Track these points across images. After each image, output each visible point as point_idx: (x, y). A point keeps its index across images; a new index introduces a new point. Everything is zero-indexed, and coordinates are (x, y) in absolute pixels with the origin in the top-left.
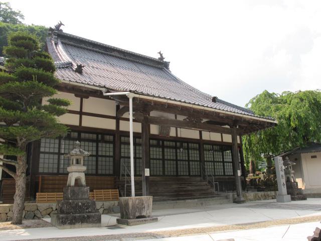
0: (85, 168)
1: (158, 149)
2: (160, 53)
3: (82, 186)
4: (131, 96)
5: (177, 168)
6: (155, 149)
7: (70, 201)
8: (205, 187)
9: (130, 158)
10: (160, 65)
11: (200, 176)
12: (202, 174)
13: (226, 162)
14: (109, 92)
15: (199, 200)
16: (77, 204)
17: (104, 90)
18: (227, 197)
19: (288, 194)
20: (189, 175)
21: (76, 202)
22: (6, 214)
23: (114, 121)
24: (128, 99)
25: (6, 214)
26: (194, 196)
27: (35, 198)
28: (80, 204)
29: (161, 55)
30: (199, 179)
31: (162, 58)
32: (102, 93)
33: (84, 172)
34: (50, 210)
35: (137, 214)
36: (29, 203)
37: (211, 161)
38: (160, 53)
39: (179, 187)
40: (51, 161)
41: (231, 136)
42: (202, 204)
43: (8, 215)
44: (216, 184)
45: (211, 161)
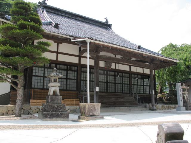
0: (59, 85)
1: (104, 76)
2: (106, 19)
3: (57, 95)
4: (88, 41)
5: (123, 88)
6: (102, 76)
7: (50, 104)
8: (132, 100)
9: (87, 81)
10: (106, 26)
11: (129, 93)
12: (130, 92)
13: (145, 86)
14: (75, 39)
15: (128, 107)
16: (54, 106)
17: (71, 38)
18: (145, 107)
19: (184, 106)
20: (123, 93)
21: (53, 105)
22: (12, 111)
23: (78, 58)
24: (87, 43)
25: (12, 111)
26: (126, 105)
27: (29, 102)
28: (56, 106)
29: (107, 20)
30: (128, 95)
31: (107, 22)
32: (71, 40)
33: (59, 87)
34: (38, 110)
35: (91, 114)
36: (26, 105)
37: (136, 85)
38: (106, 19)
39: (116, 100)
40: (36, 84)
41: (78, 58)
42: (130, 110)
43: (14, 111)
44: (139, 99)
45: (136, 85)
